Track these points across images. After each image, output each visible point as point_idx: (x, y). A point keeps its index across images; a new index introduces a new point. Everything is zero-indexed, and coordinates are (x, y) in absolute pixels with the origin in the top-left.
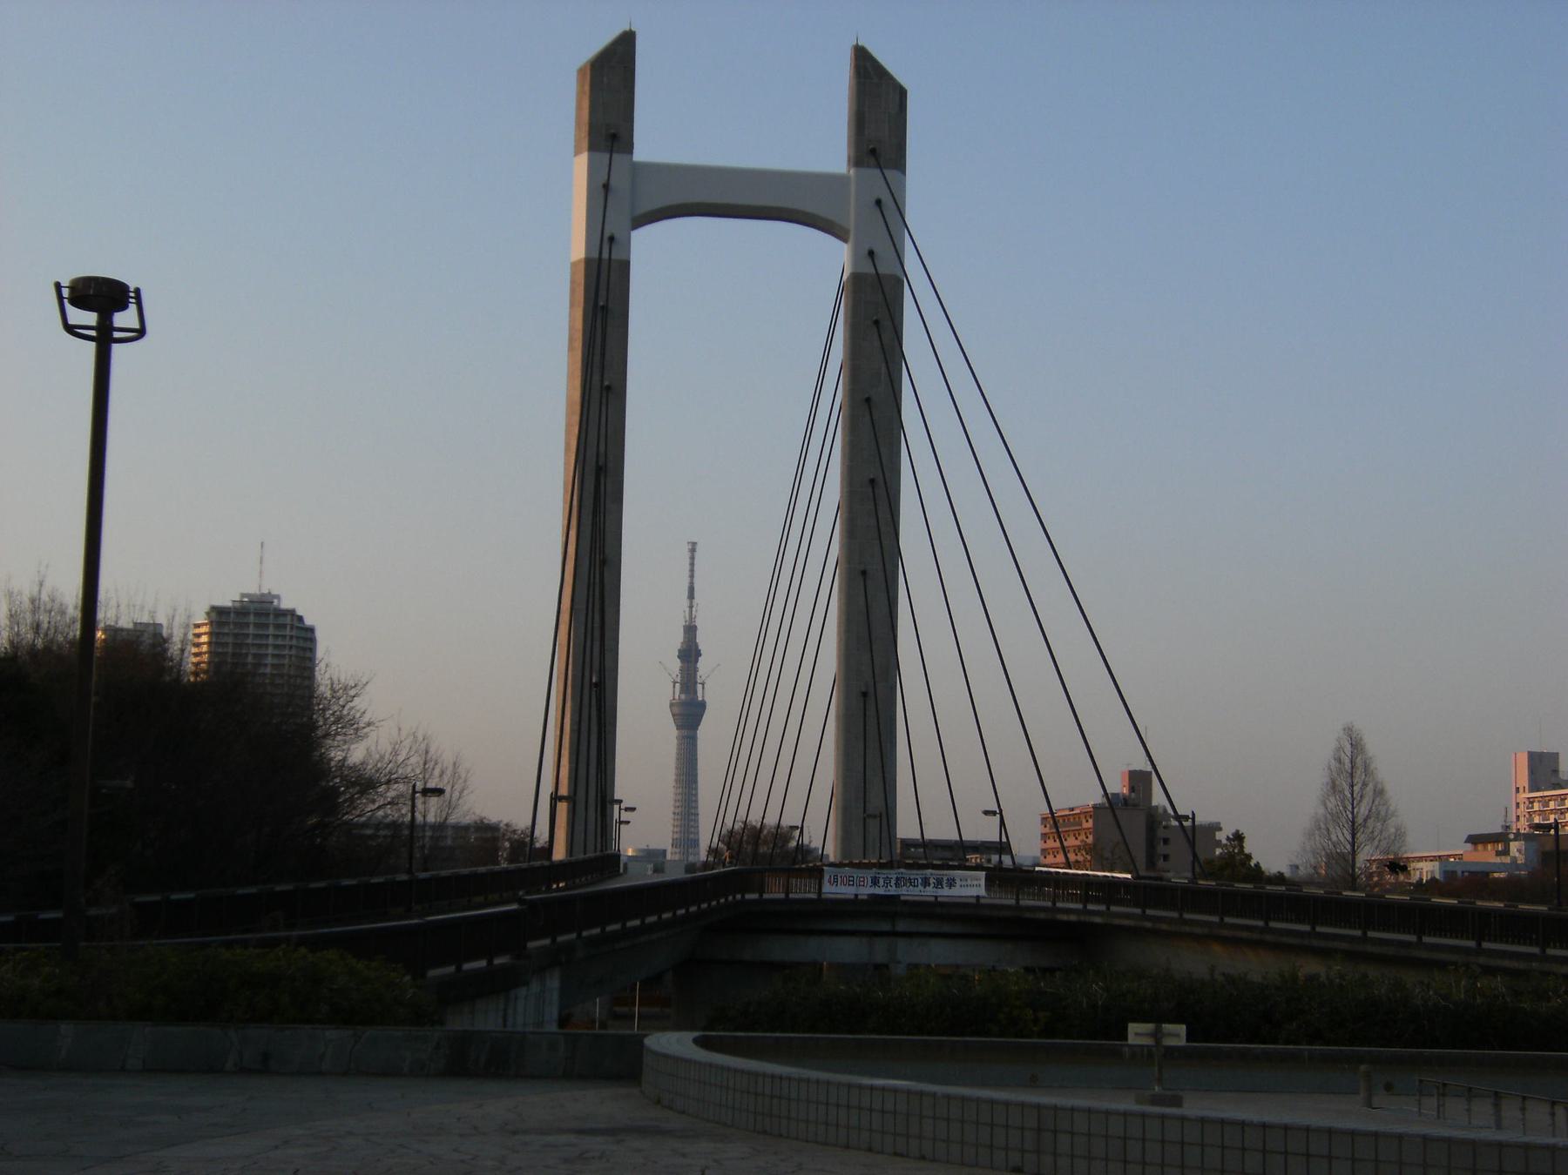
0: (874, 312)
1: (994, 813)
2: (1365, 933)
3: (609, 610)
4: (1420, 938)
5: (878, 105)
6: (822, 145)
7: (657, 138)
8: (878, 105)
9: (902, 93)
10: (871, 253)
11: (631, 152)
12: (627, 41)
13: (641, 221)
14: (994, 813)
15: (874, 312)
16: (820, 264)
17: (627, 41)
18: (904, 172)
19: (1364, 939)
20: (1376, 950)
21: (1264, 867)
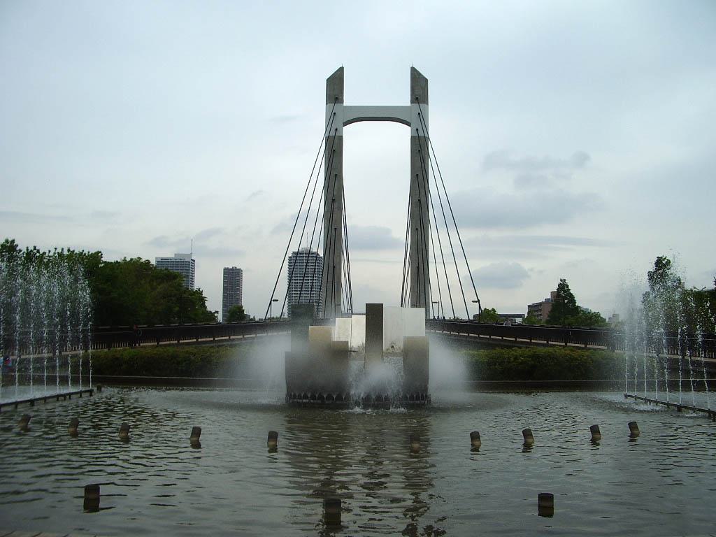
0: (420, 147)
1: (476, 302)
2: (178, 342)
3: (426, 273)
4: (566, 344)
5: (419, 86)
6: (402, 98)
7: (351, 98)
8: (419, 86)
9: (426, 80)
10: (417, 129)
11: (343, 103)
12: (341, 70)
13: (346, 124)
14: (476, 302)
15: (420, 147)
16: (401, 135)
17: (341, 70)
18: (428, 104)
19: (179, 344)
20: (506, 344)
21: (550, 310)
